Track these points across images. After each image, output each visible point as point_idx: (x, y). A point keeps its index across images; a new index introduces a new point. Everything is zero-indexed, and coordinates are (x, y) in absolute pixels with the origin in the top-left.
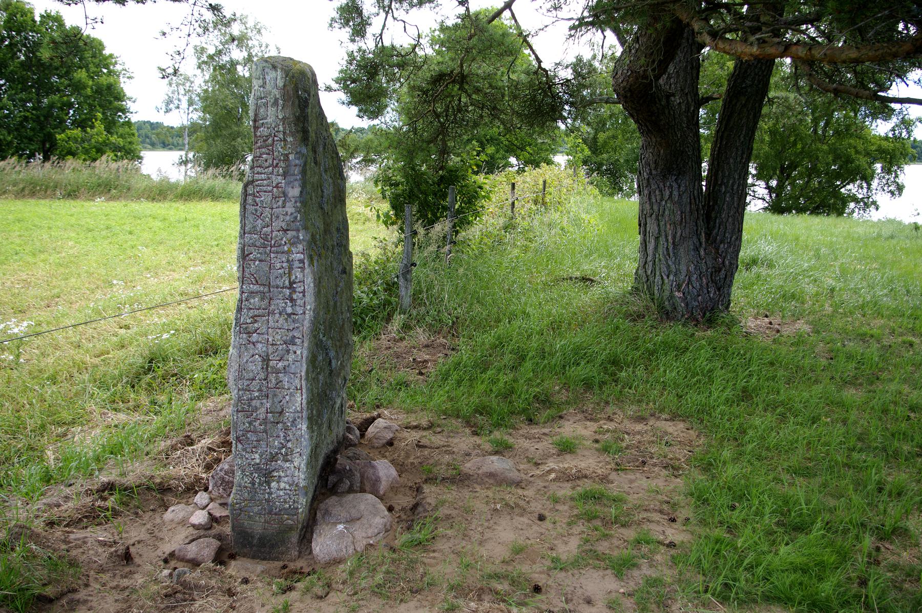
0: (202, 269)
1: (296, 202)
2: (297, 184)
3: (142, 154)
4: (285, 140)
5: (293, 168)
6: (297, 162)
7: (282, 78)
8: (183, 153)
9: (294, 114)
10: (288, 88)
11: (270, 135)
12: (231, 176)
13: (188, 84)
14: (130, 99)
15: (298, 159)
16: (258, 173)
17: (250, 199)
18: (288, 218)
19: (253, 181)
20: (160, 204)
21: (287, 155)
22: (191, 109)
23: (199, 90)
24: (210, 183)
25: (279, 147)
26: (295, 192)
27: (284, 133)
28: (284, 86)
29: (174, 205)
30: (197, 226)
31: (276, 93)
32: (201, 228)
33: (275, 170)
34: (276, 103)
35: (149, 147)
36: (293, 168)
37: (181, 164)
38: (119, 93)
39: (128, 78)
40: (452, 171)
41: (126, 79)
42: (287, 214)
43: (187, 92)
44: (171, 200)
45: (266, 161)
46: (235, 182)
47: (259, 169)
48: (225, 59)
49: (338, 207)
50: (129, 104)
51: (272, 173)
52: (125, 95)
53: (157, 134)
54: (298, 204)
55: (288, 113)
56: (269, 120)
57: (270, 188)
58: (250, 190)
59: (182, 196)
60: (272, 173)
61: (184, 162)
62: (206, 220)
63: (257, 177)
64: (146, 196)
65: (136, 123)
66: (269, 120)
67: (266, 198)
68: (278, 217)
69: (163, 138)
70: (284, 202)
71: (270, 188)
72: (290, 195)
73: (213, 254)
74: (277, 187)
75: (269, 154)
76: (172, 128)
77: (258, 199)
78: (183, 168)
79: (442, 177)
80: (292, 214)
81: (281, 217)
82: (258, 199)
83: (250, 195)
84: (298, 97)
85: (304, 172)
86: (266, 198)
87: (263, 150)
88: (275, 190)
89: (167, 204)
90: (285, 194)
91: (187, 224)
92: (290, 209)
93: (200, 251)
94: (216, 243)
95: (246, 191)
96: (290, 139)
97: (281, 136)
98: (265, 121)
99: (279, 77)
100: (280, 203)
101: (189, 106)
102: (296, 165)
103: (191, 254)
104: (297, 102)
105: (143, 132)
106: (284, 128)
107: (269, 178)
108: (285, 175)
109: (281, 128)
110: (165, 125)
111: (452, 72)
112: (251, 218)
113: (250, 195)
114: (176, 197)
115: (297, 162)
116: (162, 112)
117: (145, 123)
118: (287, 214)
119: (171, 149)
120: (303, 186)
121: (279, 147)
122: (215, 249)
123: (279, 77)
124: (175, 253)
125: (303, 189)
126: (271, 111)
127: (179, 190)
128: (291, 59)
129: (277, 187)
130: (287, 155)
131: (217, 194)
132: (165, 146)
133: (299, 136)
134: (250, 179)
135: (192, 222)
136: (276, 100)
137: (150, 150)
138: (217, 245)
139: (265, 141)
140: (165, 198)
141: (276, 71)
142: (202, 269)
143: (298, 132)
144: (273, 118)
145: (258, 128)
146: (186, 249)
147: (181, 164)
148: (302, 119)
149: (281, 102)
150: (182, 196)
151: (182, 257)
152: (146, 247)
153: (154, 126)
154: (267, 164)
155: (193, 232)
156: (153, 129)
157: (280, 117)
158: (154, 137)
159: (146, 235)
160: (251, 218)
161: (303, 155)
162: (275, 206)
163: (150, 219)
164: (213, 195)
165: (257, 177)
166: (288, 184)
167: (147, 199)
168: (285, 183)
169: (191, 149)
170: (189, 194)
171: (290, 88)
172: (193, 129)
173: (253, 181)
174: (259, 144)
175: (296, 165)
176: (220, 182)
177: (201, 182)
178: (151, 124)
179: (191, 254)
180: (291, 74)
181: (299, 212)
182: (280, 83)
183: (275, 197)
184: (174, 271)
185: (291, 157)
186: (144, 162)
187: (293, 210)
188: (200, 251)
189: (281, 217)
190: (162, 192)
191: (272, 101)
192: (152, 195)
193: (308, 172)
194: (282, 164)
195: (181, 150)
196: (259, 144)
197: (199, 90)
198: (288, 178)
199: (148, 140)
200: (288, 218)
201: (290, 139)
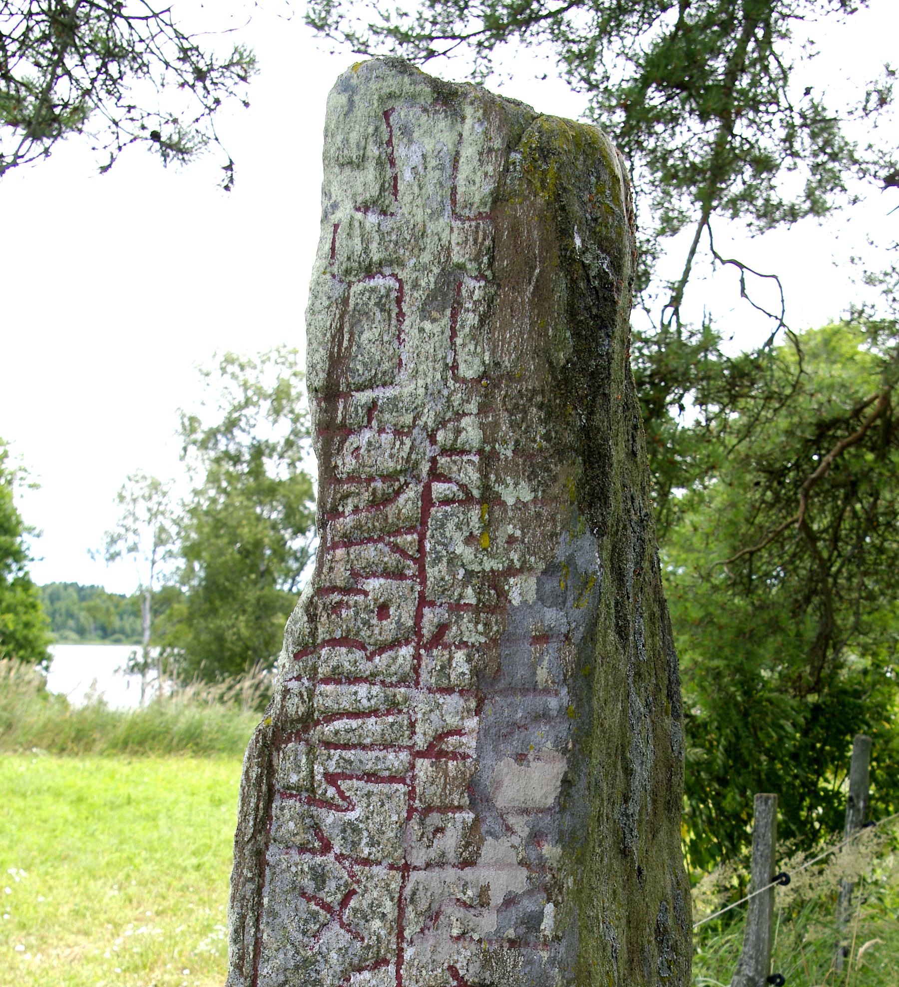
0: (154, 931)
1: (536, 837)
2: (543, 737)
3: (50, 649)
4: (489, 498)
5: (526, 651)
6: (552, 616)
7: (484, 154)
8: (140, 650)
9: (544, 354)
10: (519, 210)
11: (410, 469)
12: (238, 699)
13: (156, 498)
14: (30, 530)
15: (559, 601)
16: (336, 677)
17: (288, 816)
18: (488, 922)
19: (307, 721)
20: (75, 763)
21: (494, 582)
22: (161, 550)
23: (179, 512)
24: (192, 714)
25: (455, 538)
26: (530, 781)
27: (488, 459)
28: (498, 198)
29: (107, 764)
30: (152, 818)
31: (453, 237)
32: (162, 821)
33: (428, 663)
34: (445, 295)
35: (74, 636)
36: (526, 651)
37: (132, 670)
38: (8, 518)
39: (30, 486)
40: (844, 692)
41: (25, 490)
42: (483, 899)
43: (153, 515)
44: (101, 753)
45: (383, 610)
46: (247, 713)
47: (343, 657)
48: (243, 439)
49: (662, 836)
50: (25, 541)
51: (411, 678)
52: (19, 523)
53: (89, 610)
54: (550, 850)
55: (513, 344)
56: (406, 388)
57: (396, 760)
58: (292, 766)
59: (125, 744)
60: (411, 678)
61: (141, 668)
62: (176, 802)
63: (330, 695)
64: (46, 742)
65: (44, 588)
66: (406, 388)
67: (372, 810)
68: (433, 916)
69: (98, 617)
70: (472, 837)
71: (396, 760)
72: (501, 801)
73: (185, 889)
74: (435, 751)
75: (399, 575)
76: (123, 597)
77: (329, 818)
78: (137, 678)
79: (816, 709)
80: (510, 901)
81: (454, 914)
82: (329, 818)
83: (289, 791)
84: (568, 260)
85: (581, 677)
86: (372, 810)
87: (370, 552)
88: (424, 766)
89: (89, 763)
90: (476, 793)
91: (129, 812)
92: (500, 872)
93: (155, 881)
94: (195, 861)
95: (269, 769)
96: (515, 492)
97: (471, 476)
98: (382, 394)
99: (468, 152)
100: (450, 841)
101: (156, 545)
102: (543, 638)
103: (133, 890)
104: (560, 293)
105: (61, 605)
106: (490, 433)
107: (393, 707)
108: (481, 687)
109: (471, 433)
110: (109, 591)
111: (857, 412)
112: (289, 915)
113: (289, 791)
114: (114, 746)
115: (552, 616)
116: (101, 557)
117: (66, 586)
118: (483, 899)
119: (117, 641)
120: (576, 755)
121: (455, 538)
122: (192, 877)
123: (468, 152)
124: (94, 886)
125: (574, 765)
126: (422, 336)
127: (121, 731)
128: (518, 104)
129: (435, 751)
130: (494, 582)
131: (204, 742)
132: (106, 633)
133: (569, 474)
134: (295, 707)
135: (143, 808)
136: (450, 277)
137: (75, 642)
138: (198, 867)
139: (379, 502)
140: (88, 748)
141: (458, 117)
142: (154, 931)
143: (560, 452)
144: (432, 375)
145: (347, 431)
146: (121, 876)
147: (132, 670)
148: (582, 384)
149: (473, 288)
150: (125, 744)
151: (110, 896)
152: (28, 869)
153: (85, 594)
154: (387, 629)
155: (140, 831)
156: (83, 599)
157: (468, 371)
158: (83, 617)
159: (33, 838)
160: (289, 915)
161: (585, 581)
162: (419, 857)
163: (48, 799)
164: (195, 742)
165: (330, 695)
166: (495, 736)
167: (49, 748)
168: (484, 733)
169: (153, 642)
170: (143, 739)
171: (527, 211)
172: (164, 600)
173: (307, 721)
174: (347, 522)
175: (543, 638)
176: (214, 714)
177: (171, 710)
178: (80, 590)
179: (133, 890)
180: (532, 137)
181: (550, 891)
182: (475, 183)
183: (420, 810)
184: (87, 934)
185: (521, 589)
186: (53, 666)
187: (518, 881)
188: (155, 881)
189: (454, 914)
190: (81, 735)
191: (428, 281)
192: (59, 740)
193: (601, 676)
194: (469, 630)
195: (138, 643)
196: (347, 522)
197: (179, 512)
198: (501, 707)
199: (71, 623)
200: (488, 922)
201: (515, 492)
